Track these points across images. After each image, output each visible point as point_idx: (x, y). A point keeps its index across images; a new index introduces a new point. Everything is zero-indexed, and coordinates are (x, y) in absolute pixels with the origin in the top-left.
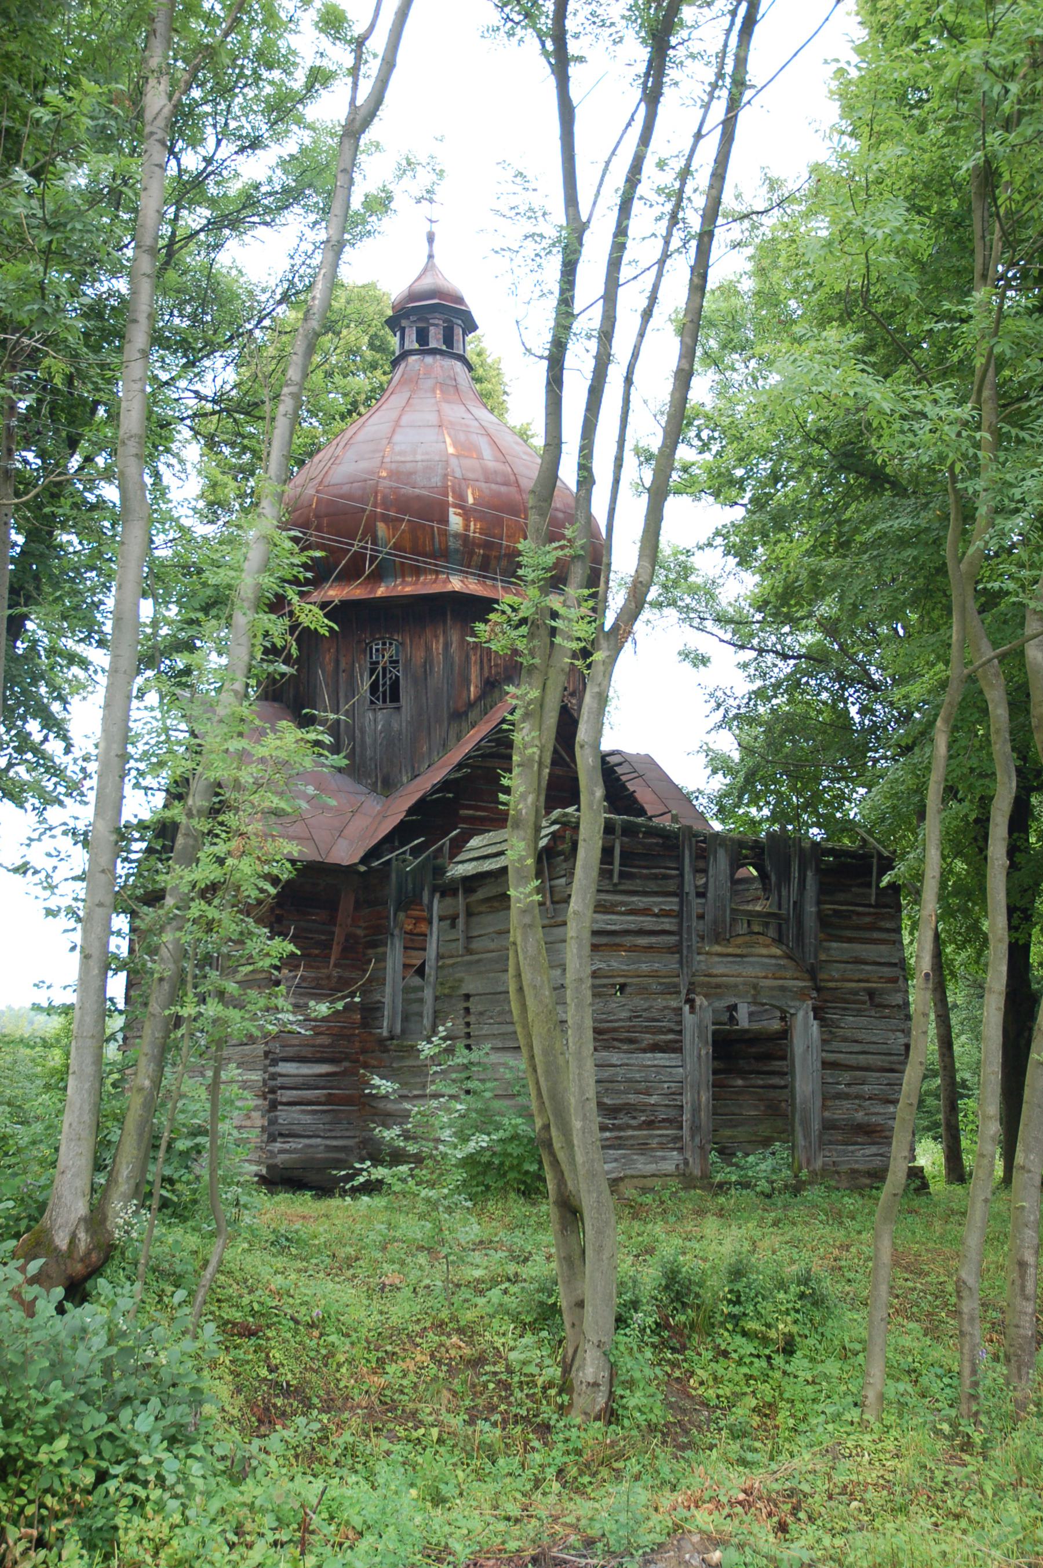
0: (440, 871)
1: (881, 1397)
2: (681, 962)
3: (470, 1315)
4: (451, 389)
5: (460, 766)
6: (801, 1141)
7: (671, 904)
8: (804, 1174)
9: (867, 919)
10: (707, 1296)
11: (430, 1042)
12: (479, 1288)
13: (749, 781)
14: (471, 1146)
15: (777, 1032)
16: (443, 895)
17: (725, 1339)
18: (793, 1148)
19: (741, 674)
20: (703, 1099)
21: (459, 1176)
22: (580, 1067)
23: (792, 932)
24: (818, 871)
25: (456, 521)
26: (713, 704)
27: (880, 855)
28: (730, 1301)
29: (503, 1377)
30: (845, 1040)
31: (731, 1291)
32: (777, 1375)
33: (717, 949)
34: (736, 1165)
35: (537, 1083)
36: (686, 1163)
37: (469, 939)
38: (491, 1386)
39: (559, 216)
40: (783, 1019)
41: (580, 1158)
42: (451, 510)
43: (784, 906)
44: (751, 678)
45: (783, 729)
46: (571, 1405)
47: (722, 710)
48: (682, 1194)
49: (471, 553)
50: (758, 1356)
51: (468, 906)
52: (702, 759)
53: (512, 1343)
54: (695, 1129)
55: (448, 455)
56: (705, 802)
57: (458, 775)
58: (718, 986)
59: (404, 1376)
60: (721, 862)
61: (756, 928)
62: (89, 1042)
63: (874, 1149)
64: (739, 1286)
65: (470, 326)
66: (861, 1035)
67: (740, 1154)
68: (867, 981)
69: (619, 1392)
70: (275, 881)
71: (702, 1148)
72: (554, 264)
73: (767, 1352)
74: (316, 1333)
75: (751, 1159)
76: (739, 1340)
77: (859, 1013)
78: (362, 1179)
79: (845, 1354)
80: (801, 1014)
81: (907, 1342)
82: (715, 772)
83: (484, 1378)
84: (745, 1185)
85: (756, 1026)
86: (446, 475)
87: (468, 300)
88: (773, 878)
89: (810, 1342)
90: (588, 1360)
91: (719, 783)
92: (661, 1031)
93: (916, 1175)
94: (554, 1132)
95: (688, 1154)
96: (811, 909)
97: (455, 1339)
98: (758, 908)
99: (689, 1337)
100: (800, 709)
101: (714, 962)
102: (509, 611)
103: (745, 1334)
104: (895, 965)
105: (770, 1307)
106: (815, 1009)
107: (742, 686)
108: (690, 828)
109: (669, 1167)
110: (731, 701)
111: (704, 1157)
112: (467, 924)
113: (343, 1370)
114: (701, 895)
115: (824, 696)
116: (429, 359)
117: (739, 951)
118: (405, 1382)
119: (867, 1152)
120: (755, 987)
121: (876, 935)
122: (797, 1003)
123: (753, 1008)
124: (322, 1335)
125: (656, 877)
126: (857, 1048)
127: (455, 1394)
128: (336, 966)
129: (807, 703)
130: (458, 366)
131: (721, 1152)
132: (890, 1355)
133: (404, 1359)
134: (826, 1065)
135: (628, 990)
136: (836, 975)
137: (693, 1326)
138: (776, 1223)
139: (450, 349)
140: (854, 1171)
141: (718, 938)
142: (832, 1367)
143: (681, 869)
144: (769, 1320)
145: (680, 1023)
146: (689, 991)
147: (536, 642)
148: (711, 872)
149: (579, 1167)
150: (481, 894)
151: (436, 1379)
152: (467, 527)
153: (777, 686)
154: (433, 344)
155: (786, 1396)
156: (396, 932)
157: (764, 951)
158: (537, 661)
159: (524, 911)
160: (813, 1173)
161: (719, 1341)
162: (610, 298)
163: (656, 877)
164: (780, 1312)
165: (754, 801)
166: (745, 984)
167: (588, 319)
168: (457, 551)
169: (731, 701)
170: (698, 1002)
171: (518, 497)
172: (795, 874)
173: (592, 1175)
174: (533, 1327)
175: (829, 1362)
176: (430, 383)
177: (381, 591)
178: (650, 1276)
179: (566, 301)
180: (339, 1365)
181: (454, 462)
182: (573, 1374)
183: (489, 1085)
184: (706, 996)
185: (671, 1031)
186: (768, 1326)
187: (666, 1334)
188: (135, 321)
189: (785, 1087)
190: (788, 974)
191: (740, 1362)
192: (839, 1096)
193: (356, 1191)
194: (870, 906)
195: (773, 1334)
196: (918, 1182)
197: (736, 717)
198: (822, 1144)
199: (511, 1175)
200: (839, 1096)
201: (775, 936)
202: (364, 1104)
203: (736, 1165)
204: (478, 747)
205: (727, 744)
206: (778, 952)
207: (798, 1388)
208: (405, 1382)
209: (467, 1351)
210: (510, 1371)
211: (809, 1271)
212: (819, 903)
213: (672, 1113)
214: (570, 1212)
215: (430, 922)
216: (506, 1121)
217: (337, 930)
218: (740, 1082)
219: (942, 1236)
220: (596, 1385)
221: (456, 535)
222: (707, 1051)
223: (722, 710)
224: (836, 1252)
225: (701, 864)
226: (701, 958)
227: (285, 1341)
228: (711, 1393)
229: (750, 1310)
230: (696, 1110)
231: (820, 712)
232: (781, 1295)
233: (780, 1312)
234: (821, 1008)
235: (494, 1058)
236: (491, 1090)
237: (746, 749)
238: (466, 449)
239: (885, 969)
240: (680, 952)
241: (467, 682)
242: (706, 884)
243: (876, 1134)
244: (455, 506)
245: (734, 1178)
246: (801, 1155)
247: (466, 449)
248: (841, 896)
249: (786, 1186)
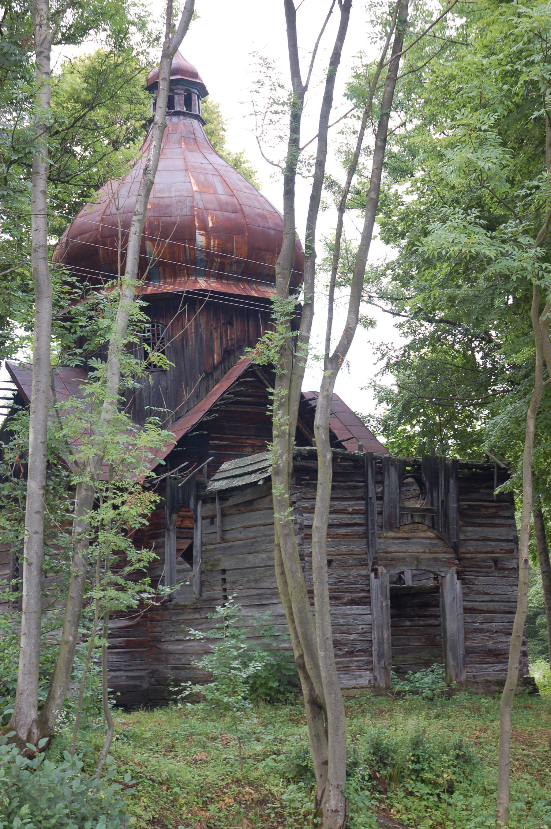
0: (201, 486)
1: (507, 811)
2: (367, 544)
3: (256, 774)
4: (191, 140)
5: (210, 412)
6: (451, 662)
7: (360, 505)
8: (454, 684)
9: (491, 511)
10: (398, 758)
11: (224, 606)
12: (257, 758)
13: (406, 406)
14: (251, 670)
15: (432, 588)
16: (204, 502)
17: (410, 784)
18: (446, 667)
19: (397, 332)
20: (385, 636)
21: (246, 688)
22: (322, 619)
23: (441, 521)
24: (458, 479)
25: (201, 239)
26: (379, 355)
27: (499, 467)
28: (413, 762)
29: (280, 810)
30: (479, 593)
31: (413, 755)
32: (444, 805)
33: (391, 534)
34: (407, 680)
35: (295, 629)
36: (375, 679)
37: (224, 531)
38: (273, 815)
39: (289, 86)
40: (435, 579)
41: (323, 674)
42: (198, 232)
43: (435, 503)
44: (405, 334)
45: (430, 370)
46: (322, 824)
47: (386, 359)
48: (373, 699)
49: (212, 261)
50: (432, 795)
51: (222, 510)
52: (371, 392)
53: (282, 790)
54: (381, 656)
55: (193, 192)
56: (374, 423)
57: (210, 418)
58: (393, 559)
59: (220, 812)
60: (393, 476)
61: (417, 520)
62: (33, 615)
63: (500, 667)
64: (418, 752)
65: (203, 92)
66: (489, 589)
67: (410, 672)
68: (493, 552)
69: (351, 815)
70: (144, 516)
71: (385, 668)
72: (287, 119)
73: (437, 791)
74: (164, 788)
75: (418, 675)
76: (419, 784)
77: (487, 574)
78: (187, 693)
79: (485, 792)
80: (448, 576)
81: (523, 785)
82: (380, 401)
83: (268, 811)
84: (415, 692)
85: (417, 584)
86: (192, 207)
87: (200, 74)
88: (427, 485)
89: (464, 785)
90: (332, 796)
91: (384, 409)
92: (356, 591)
93: (529, 683)
94: (306, 659)
95: (376, 673)
96: (453, 505)
97: (247, 789)
98: (418, 506)
99: (389, 784)
100: (441, 356)
101: (389, 543)
102: (267, 341)
103: (423, 781)
104: (511, 541)
105: (438, 764)
106: (458, 573)
107: (400, 342)
108: (371, 454)
109: (364, 682)
110: (392, 353)
111: (387, 674)
112: (222, 522)
113: (184, 809)
114: (380, 498)
115: (457, 346)
117: (405, 535)
118: (221, 815)
119: (496, 668)
120: (417, 559)
121: (497, 521)
122: (445, 569)
123: (414, 572)
124: (168, 789)
125: (349, 488)
126: (487, 598)
127: (251, 821)
129: (446, 352)
130: (195, 123)
131: (397, 671)
132: (513, 793)
133: (218, 802)
134: (467, 610)
135: (334, 564)
136: (471, 549)
137: (391, 778)
138: (437, 717)
139: (189, 112)
140: (487, 681)
141: (391, 527)
142: (477, 800)
143: (366, 482)
144: (438, 773)
145: (368, 585)
146: (374, 564)
147: (284, 360)
148: (386, 483)
149: (323, 680)
150: (232, 501)
151: (239, 813)
152: (208, 243)
153: (423, 342)
155: (450, 817)
156: (171, 527)
157: (423, 535)
158: (285, 372)
159: (284, 526)
160: (460, 683)
161: (407, 785)
162: (322, 138)
163: (349, 488)
164: (445, 767)
165: (409, 422)
166: (411, 557)
167: (310, 151)
168: (202, 260)
169: (392, 353)
170: (380, 571)
171: (243, 221)
172: (442, 482)
173: (331, 684)
174: (295, 780)
175: (475, 797)
176: (176, 137)
178: (363, 750)
179: (294, 142)
180: (182, 806)
181: (197, 197)
182: (322, 806)
183: (243, 631)
184: (385, 566)
185: (362, 590)
186: (438, 776)
187: (375, 783)
188: (37, 173)
189: (439, 625)
190: (439, 550)
191: (421, 799)
192: (476, 631)
193: (185, 700)
194: (493, 501)
195: (440, 781)
196: (531, 688)
197: (397, 363)
198: (465, 664)
199: (262, 690)
200: (476, 631)
201: (430, 524)
202: (152, 647)
203: (407, 680)
204: (222, 398)
205: (390, 381)
206: (432, 535)
207: (457, 812)
208: (221, 815)
209: (256, 796)
210: (283, 807)
211: (461, 741)
212: (458, 500)
213: (365, 646)
214: (318, 706)
215: (196, 521)
216: (256, 654)
218: (408, 623)
219: (546, 722)
220: (336, 811)
222: (387, 603)
223: (386, 359)
224: (478, 733)
225: (379, 478)
226: (381, 541)
227: (148, 792)
228: (404, 817)
229: (426, 766)
230: (381, 643)
231: (454, 357)
232: (444, 757)
233: (445, 767)
234: (462, 572)
235: (244, 612)
236: (244, 634)
237: (402, 386)
238: (206, 187)
239: (504, 544)
240: (367, 537)
241: (212, 351)
242: (383, 491)
243: (499, 655)
245: (407, 688)
246: (452, 672)
247: (206, 187)
248: (473, 496)
249: (442, 693)
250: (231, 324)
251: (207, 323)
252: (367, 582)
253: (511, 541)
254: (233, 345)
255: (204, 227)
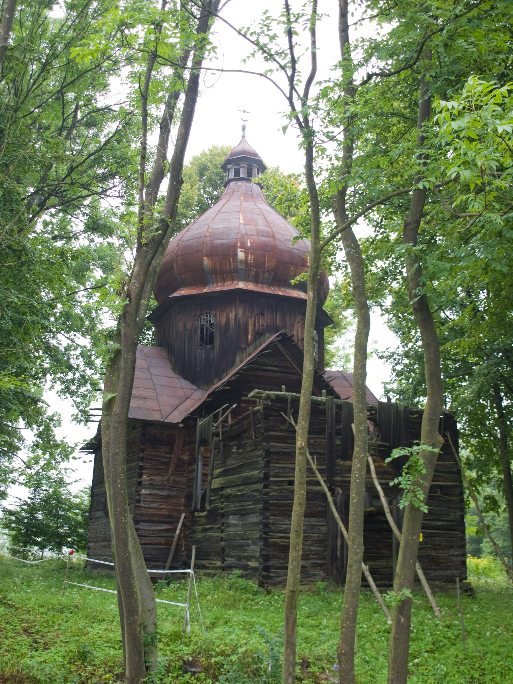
25: (241, 255)
42: (239, 249)
87: (260, 154)
104: (454, 473)
116: (240, 183)
128: (172, 474)
152: (247, 257)
154: (242, 175)
168: (242, 269)
177: (205, 290)
181: (242, 227)
217: (173, 456)
221: (241, 262)
244: (241, 247)
250: (263, 315)
251: (244, 313)
252: (140, 532)
253: (454, 473)
254: (263, 329)
255: (243, 246)
